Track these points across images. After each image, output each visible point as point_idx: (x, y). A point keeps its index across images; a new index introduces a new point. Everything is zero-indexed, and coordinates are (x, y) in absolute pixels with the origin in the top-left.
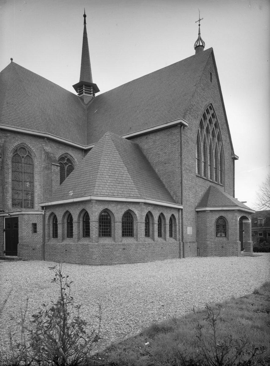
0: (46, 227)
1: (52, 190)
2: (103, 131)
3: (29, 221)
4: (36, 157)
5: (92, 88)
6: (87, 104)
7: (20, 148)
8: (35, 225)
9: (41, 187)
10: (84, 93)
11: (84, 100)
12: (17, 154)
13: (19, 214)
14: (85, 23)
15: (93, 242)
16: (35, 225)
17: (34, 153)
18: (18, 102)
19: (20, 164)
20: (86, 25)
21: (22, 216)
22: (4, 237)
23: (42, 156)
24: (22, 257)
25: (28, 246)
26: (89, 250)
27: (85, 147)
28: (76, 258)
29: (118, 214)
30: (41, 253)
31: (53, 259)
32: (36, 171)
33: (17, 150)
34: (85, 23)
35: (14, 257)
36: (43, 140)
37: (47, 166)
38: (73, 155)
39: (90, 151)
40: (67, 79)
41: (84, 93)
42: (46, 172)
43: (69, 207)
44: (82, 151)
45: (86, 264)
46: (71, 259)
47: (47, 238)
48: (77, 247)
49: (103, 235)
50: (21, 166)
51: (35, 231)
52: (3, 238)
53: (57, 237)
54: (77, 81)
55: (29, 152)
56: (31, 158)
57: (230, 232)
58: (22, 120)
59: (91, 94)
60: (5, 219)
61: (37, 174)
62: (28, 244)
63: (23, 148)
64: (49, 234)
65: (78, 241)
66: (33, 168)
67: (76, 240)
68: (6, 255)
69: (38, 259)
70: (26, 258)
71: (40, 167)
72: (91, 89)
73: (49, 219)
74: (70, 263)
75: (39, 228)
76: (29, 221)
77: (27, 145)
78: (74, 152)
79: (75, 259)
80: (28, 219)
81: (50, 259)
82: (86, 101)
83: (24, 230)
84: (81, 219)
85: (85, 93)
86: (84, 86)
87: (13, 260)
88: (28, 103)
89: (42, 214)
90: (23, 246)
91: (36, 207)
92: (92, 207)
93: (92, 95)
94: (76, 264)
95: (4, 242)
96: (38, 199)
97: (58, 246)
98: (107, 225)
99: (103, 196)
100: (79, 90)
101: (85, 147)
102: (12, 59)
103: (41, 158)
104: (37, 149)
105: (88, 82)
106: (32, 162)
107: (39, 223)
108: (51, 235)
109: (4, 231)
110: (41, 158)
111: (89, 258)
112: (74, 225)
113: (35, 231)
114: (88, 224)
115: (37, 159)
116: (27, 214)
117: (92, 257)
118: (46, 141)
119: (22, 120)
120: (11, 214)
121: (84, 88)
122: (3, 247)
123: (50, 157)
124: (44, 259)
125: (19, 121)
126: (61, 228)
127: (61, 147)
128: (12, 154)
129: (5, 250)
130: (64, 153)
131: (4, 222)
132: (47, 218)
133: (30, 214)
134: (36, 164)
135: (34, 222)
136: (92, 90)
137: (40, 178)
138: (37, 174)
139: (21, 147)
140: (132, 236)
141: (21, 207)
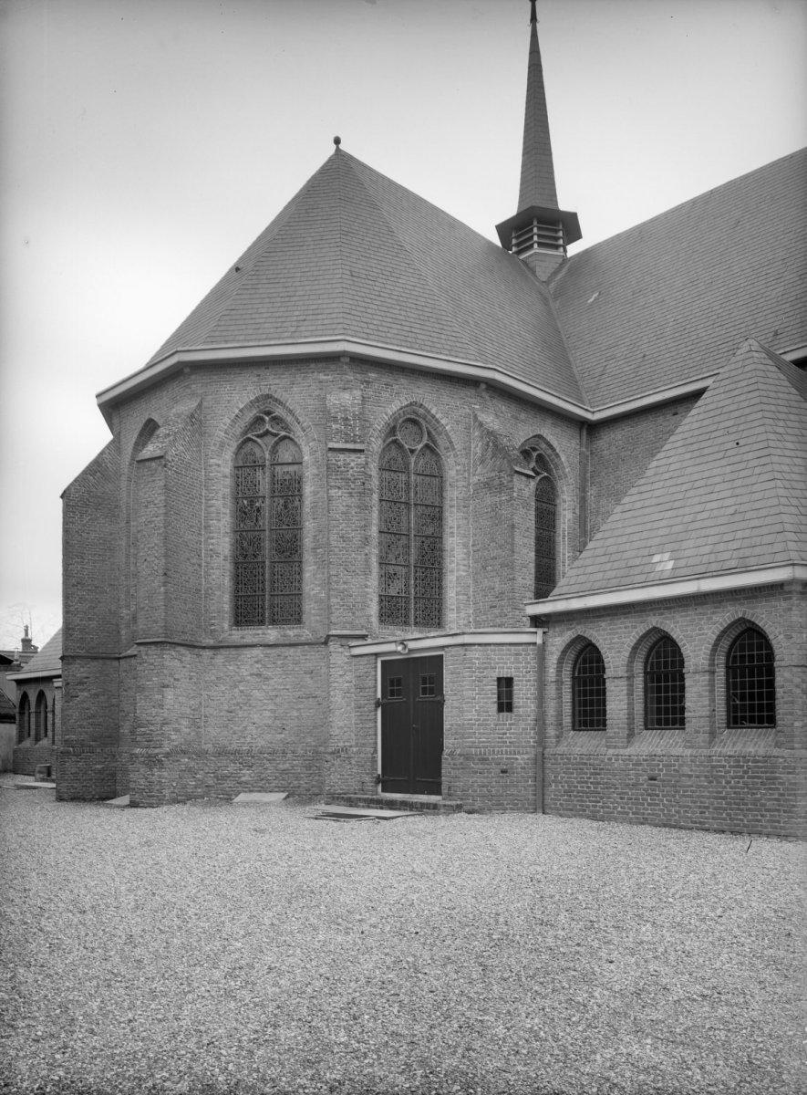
0: (551, 691)
1: (513, 562)
2: (646, 358)
3: (486, 668)
4: (454, 449)
5: (561, 227)
6: (547, 283)
7: (403, 422)
8: (506, 684)
9: (468, 554)
10: (536, 246)
11: (538, 269)
12: (395, 442)
13: (447, 646)
14: (534, 19)
15: (796, 745)
16: (506, 684)
17: (447, 435)
18: (380, 271)
19: (403, 477)
20: (538, 25)
21: (461, 651)
22: (376, 726)
23: (473, 446)
24: (462, 799)
25: (484, 760)
26: (776, 778)
27: (593, 413)
28: (707, 808)
29: (698, 643)
30: (530, 786)
31: (585, 810)
32: (452, 500)
33: (394, 427)
34: (534, 19)
35: (433, 799)
36: (473, 391)
37: (492, 479)
38: (555, 444)
39: (700, 403)
40: (483, 200)
41: (536, 246)
42: (489, 500)
43: (662, 614)
44: (581, 429)
45: (760, 834)
46: (678, 812)
47: (551, 732)
48: (713, 767)
49: (659, 722)
50: (408, 484)
51: (505, 705)
52: (371, 732)
53: (605, 725)
54: (509, 208)
55: (429, 433)
56: (437, 455)
57: (781, 709)
58: (405, 328)
59: (557, 247)
60: (382, 662)
61: (454, 510)
62: (485, 754)
63: (413, 420)
64: (559, 715)
65: (710, 742)
66: (442, 489)
67: (703, 737)
68: (383, 791)
69: (518, 806)
70: (478, 805)
71: (465, 484)
72: (557, 231)
73: (560, 661)
74: (675, 827)
75: (523, 694)
76: (486, 668)
77: (426, 410)
78: (558, 430)
79: (701, 813)
80: (484, 663)
81: (571, 810)
82: (545, 272)
83: (469, 702)
84: (721, 660)
85: (540, 245)
86: (535, 223)
87: (422, 809)
88: (410, 274)
89: (535, 644)
90: (467, 759)
91: (451, 622)
92: (790, 609)
93: (562, 249)
94: (707, 830)
95: (376, 743)
96: (457, 594)
97: (610, 759)
98: (667, 692)
99: (701, 576)
100: (515, 237)
101: (593, 413)
102: (337, 141)
103: (468, 455)
104: (458, 422)
105: (550, 206)
106: (440, 468)
107: (523, 676)
108: (567, 720)
109: (378, 704)
110: (468, 455)
111: (778, 810)
112: (687, 683)
113: (505, 705)
114: (598, 684)
115: (456, 456)
116: (480, 645)
117: (794, 806)
118: (484, 394)
119: (405, 328)
120: (412, 645)
121: (535, 230)
122: (374, 761)
123: (504, 448)
124: (541, 806)
125: (396, 332)
126: (625, 692)
127: (523, 416)
128: (380, 442)
129: (380, 772)
130: (531, 435)
131: (376, 675)
132: (552, 660)
133: (489, 644)
134: (452, 473)
135: (505, 673)
136: (561, 234)
137: (465, 521)
138: (454, 510)
139: (409, 416)
140: (735, 718)
141: (406, 623)
